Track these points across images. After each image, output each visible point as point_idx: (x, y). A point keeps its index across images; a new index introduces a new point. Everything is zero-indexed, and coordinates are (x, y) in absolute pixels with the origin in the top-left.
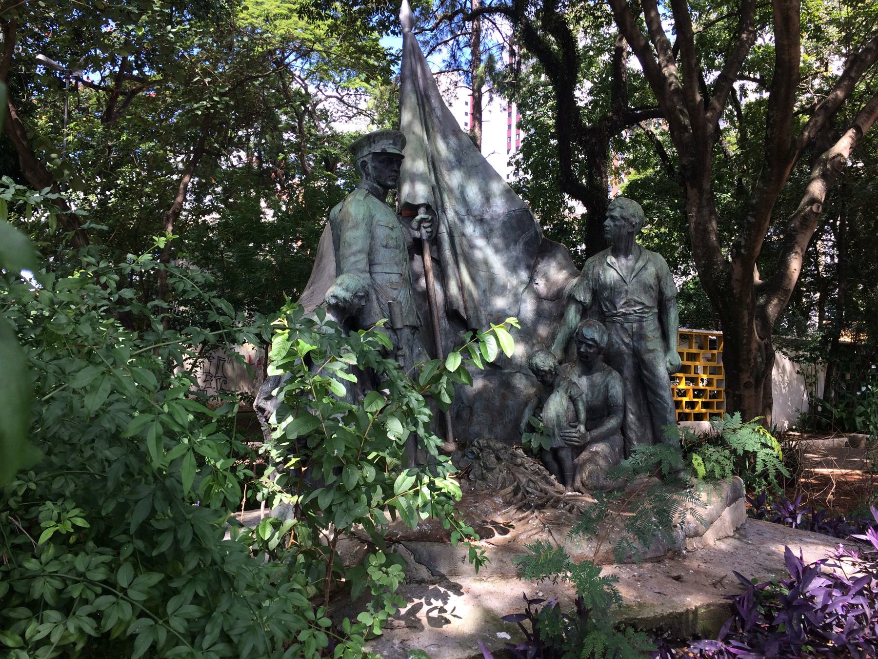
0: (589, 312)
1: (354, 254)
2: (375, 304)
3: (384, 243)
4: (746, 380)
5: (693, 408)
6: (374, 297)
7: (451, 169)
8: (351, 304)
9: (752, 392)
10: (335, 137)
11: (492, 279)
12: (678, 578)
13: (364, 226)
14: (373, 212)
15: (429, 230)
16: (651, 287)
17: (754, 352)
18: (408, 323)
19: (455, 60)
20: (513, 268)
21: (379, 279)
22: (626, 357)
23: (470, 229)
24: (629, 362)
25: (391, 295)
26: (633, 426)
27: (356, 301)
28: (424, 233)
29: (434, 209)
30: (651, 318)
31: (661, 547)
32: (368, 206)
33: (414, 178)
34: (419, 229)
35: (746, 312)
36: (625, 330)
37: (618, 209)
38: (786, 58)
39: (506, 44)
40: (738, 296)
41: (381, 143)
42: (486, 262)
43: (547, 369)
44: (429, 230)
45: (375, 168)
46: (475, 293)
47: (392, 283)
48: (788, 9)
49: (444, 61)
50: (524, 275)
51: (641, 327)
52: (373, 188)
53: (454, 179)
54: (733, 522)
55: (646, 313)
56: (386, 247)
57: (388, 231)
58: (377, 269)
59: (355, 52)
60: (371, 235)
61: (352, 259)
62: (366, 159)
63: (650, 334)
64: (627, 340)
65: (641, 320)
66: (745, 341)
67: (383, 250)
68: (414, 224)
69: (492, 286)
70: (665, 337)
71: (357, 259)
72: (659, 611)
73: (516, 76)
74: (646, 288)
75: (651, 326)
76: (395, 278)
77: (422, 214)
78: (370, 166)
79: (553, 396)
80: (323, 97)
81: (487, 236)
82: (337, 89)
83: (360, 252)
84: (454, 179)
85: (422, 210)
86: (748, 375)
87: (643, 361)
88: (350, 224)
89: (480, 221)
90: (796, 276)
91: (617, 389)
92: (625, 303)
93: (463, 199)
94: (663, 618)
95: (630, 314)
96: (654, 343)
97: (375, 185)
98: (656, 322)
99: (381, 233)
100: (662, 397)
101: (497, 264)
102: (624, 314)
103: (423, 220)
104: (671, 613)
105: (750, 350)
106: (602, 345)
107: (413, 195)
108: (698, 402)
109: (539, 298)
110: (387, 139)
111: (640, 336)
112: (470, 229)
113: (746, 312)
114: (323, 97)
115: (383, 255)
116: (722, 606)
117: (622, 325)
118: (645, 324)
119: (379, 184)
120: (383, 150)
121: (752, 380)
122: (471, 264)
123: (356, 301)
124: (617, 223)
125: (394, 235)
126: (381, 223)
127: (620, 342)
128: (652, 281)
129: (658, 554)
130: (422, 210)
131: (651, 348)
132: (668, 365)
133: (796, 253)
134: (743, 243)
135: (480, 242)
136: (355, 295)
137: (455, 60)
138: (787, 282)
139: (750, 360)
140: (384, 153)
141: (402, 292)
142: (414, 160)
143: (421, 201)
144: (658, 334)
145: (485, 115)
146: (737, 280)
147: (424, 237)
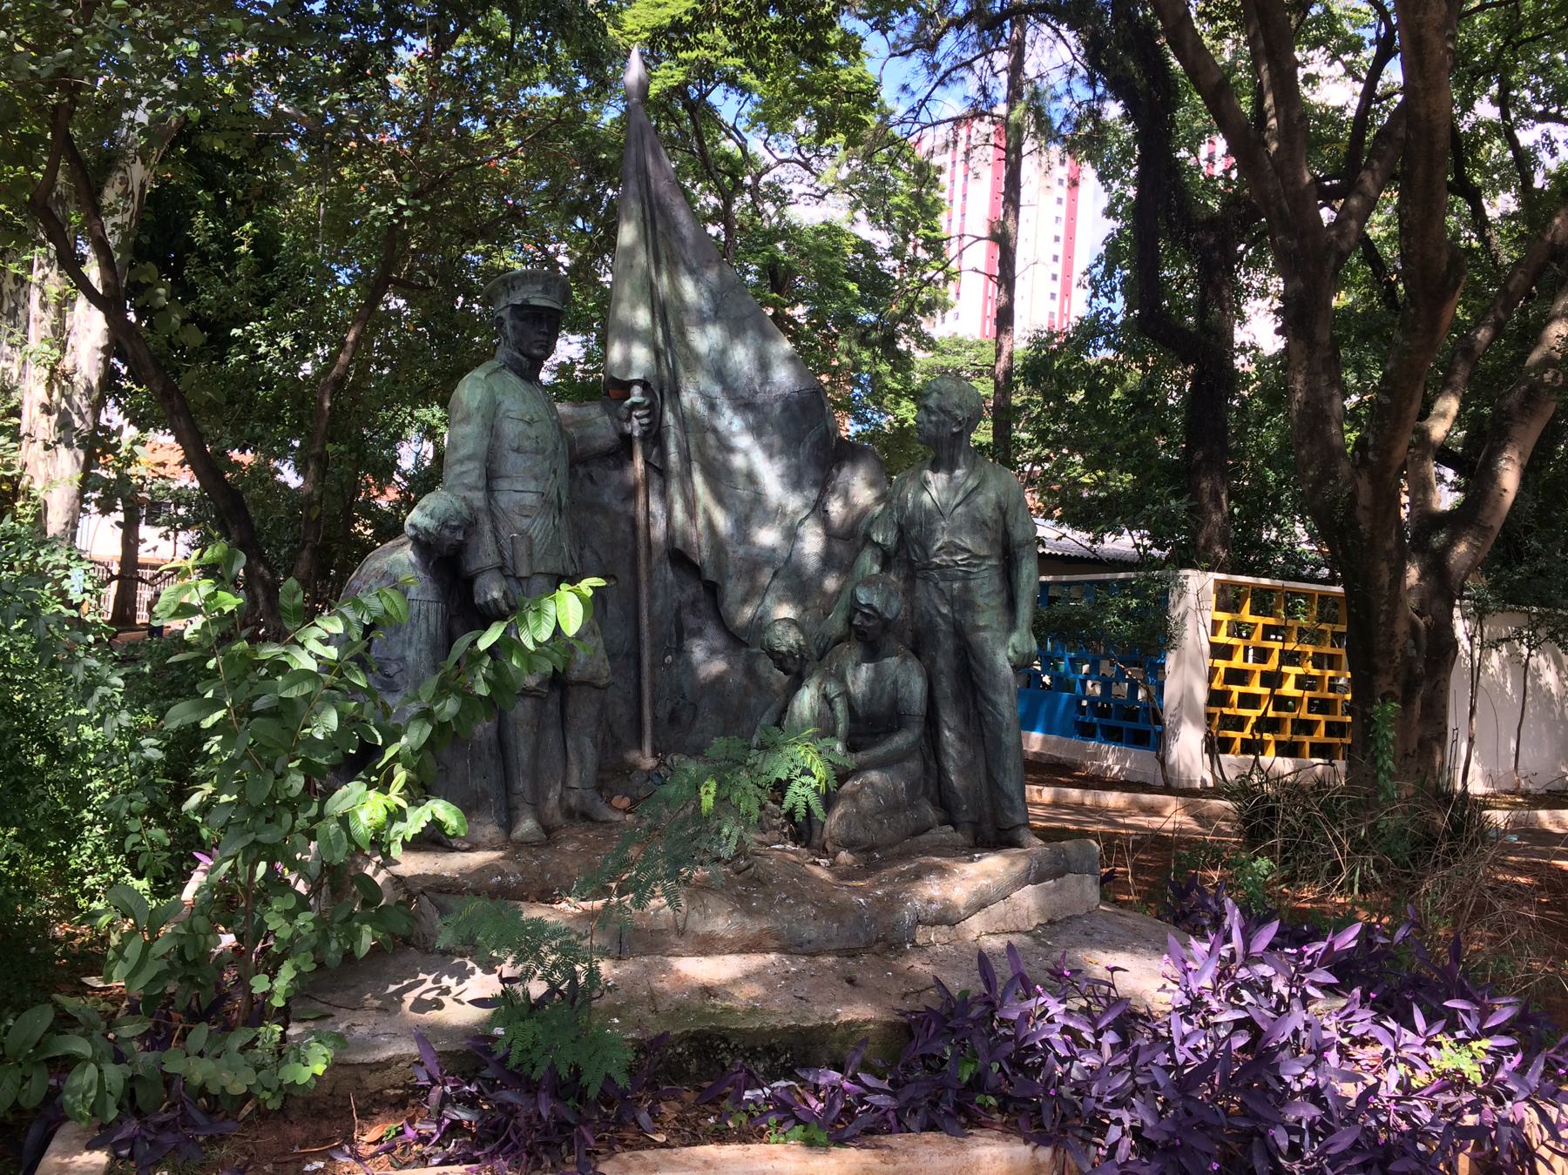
0: (894, 561)
1: (461, 462)
2: (488, 538)
3: (515, 445)
4: (1385, 689)
5: (1310, 733)
6: (487, 528)
7: (702, 321)
8: (439, 538)
9: (1393, 707)
10: (788, 232)
11: (758, 498)
12: (851, 981)
13: (479, 419)
14: (499, 397)
15: (645, 421)
16: (984, 523)
17: (1402, 638)
18: (542, 569)
19: (986, 96)
20: (795, 482)
21: (504, 500)
22: (941, 636)
23: (731, 423)
24: (948, 644)
25: (518, 525)
26: (951, 751)
27: (446, 532)
28: (635, 427)
29: (662, 388)
30: (986, 574)
31: (861, 935)
32: (490, 389)
33: (630, 334)
34: (629, 419)
35: (1384, 566)
36: (941, 592)
37: (935, 395)
38: (1422, 111)
39: (1077, 65)
40: (1367, 536)
41: (523, 289)
42: (751, 477)
43: (784, 649)
44: (645, 421)
45: (514, 327)
46: (722, 521)
47: (523, 507)
48: (1420, 25)
49: (966, 98)
50: (813, 494)
51: (966, 589)
52: (513, 358)
53: (705, 340)
54: (1041, 910)
55: (975, 566)
56: (518, 450)
57: (522, 426)
58: (504, 484)
59: (797, 92)
60: (492, 429)
61: (458, 469)
62: (503, 314)
63: (980, 601)
64: (945, 610)
65: (967, 577)
66: (1382, 618)
67: (512, 456)
68: (623, 412)
69: (752, 509)
70: (1011, 605)
71: (464, 468)
72: (773, 1021)
73: (1096, 122)
74: (977, 525)
75: (986, 587)
76: (530, 499)
77: (636, 395)
78: (508, 324)
79: (800, 692)
80: (773, 161)
81: (757, 430)
82: (799, 149)
83: (469, 458)
84: (705, 340)
85: (637, 390)
86: (1390, 679)
87: (969, 645)
88: (459, 416)
89: (744, 404)
90: (1509, 498)
91: (916, 686)
92: (941, 548)
93: (720, 374)
94: (774, 1031)
95: (948, 566)
96: (988, 616)
97: (516, 354)
98: (997, 580)
99: (510, 429)
100: (994, 705)
101: (770, 475)
102: (939, 566)
103: (635, 406)
104: (790, 1027)
105: (1393, 635)
106: (888, 616)
107: (627, 363)
108: (1318, 722)
109: (830, 534)
110: (533, 283)
111: (964, 603)
112: (731, 423)
113: (1384, 566)
114: (773, 161)
115: (513, 463)
116: (886, 1024)
117: (936, 584)
118: (972, 583)
119: (521, 353)
120: (526, 300)
121: (1397, 690)
122: (719, 476)
123: (446, 532)
124: (933, 418)
125: (532, 433)
126: (511, 415)
127: (933, 612)
128: (989, 513)
129: (854, 945)
130: (637, 390)
131: (982, 624)
132: (1011, 653)
133: (1509, 459)
134: (1371, 442)
135: (744, 441)
136: (444, 524)
137: (986, 96)
138: (1488, 511)
139: (1392, 653)
140: (525, 306)
141: (539, 521)
142: (633, 307)
143: (636, 376)
144: (996, 601)
145: (1025, 195)
146: (1365, 508)
147: (636, 433)
